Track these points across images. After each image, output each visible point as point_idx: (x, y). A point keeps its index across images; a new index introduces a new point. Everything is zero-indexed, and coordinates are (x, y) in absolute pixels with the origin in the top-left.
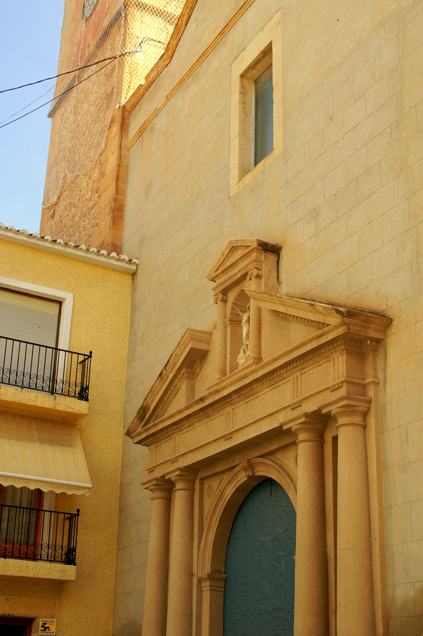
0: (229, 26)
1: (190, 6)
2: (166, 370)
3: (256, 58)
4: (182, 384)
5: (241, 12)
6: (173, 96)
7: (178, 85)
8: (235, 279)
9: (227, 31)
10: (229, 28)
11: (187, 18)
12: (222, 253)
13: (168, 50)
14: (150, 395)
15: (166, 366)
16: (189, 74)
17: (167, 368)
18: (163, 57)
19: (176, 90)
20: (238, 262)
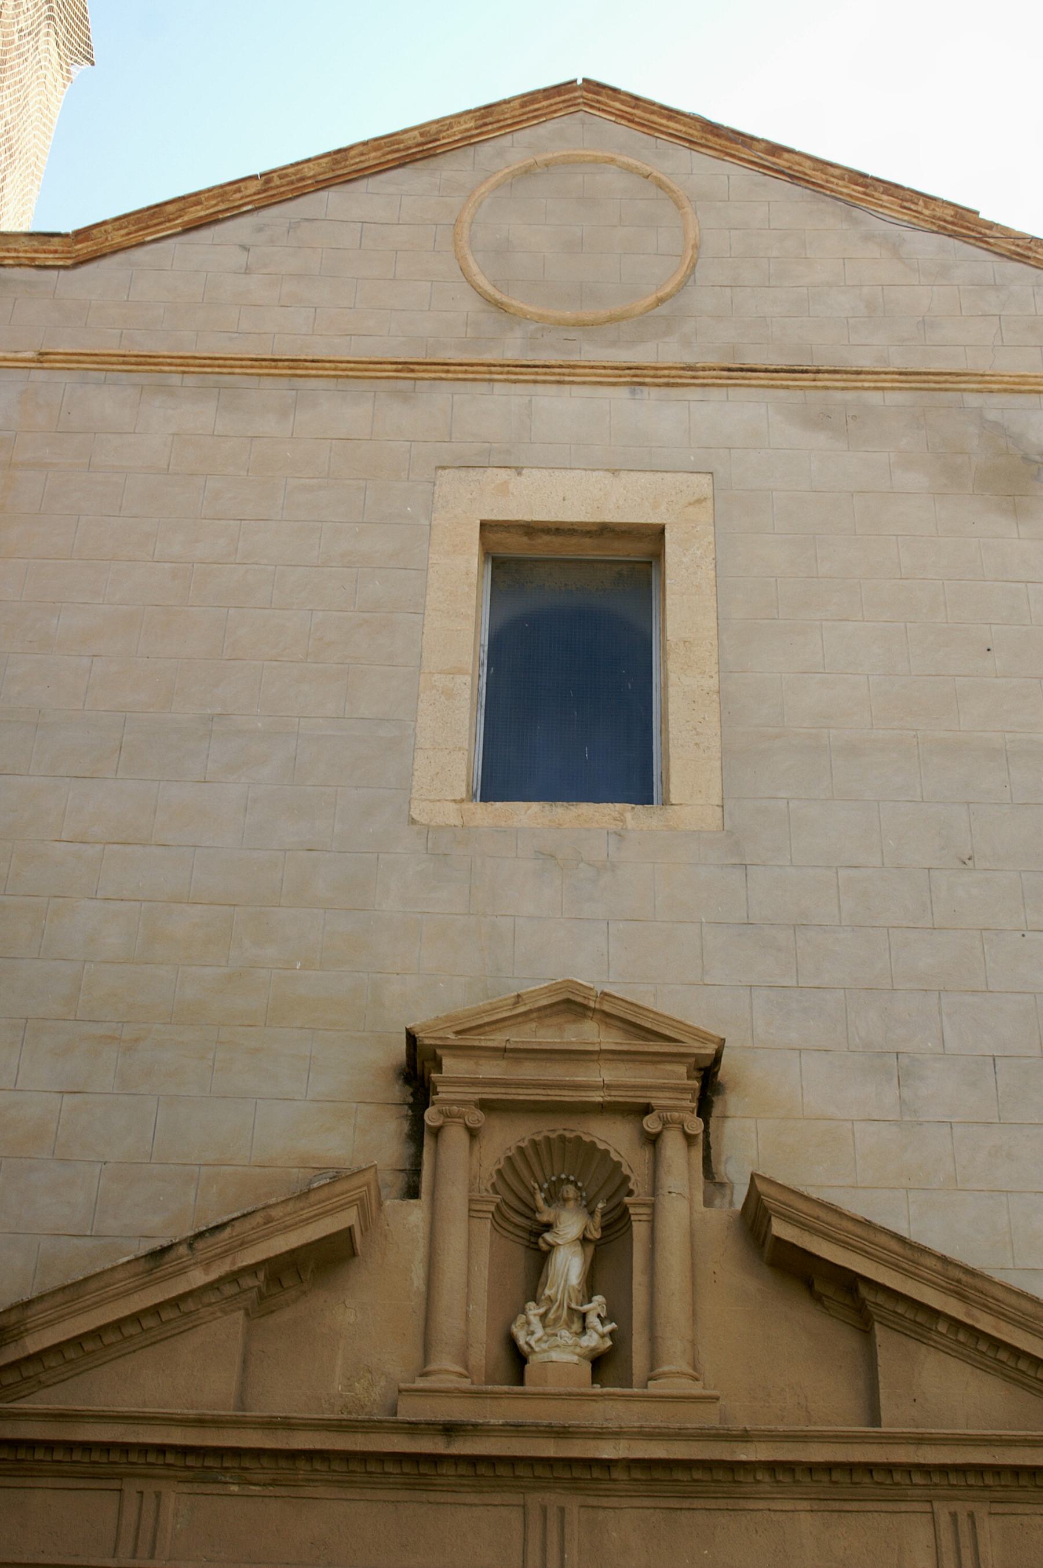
0: (448, 372)
1: (233, 201)
2: (190, 1246)
3: (572, 524)
4: (216, 1319)
5: (516, 374)
6: (69, 369)
7: (121, 359)
8: (567, 1099)
9: (433, 375)
10: (443, 375)
11: (201, 218)
12: (519, 996)
13: (80, 237)
14: (59, 1298)
15: (200, 1235)
16: (188, 365)
17: (200, 1245)
18: (46, 239)
19: (98, 363)
20: (595, 1057)
